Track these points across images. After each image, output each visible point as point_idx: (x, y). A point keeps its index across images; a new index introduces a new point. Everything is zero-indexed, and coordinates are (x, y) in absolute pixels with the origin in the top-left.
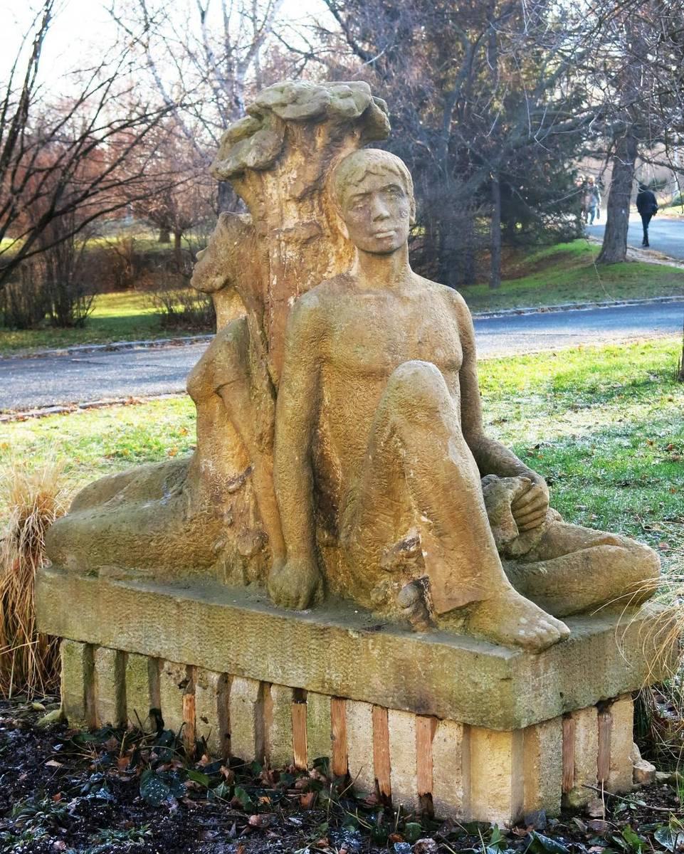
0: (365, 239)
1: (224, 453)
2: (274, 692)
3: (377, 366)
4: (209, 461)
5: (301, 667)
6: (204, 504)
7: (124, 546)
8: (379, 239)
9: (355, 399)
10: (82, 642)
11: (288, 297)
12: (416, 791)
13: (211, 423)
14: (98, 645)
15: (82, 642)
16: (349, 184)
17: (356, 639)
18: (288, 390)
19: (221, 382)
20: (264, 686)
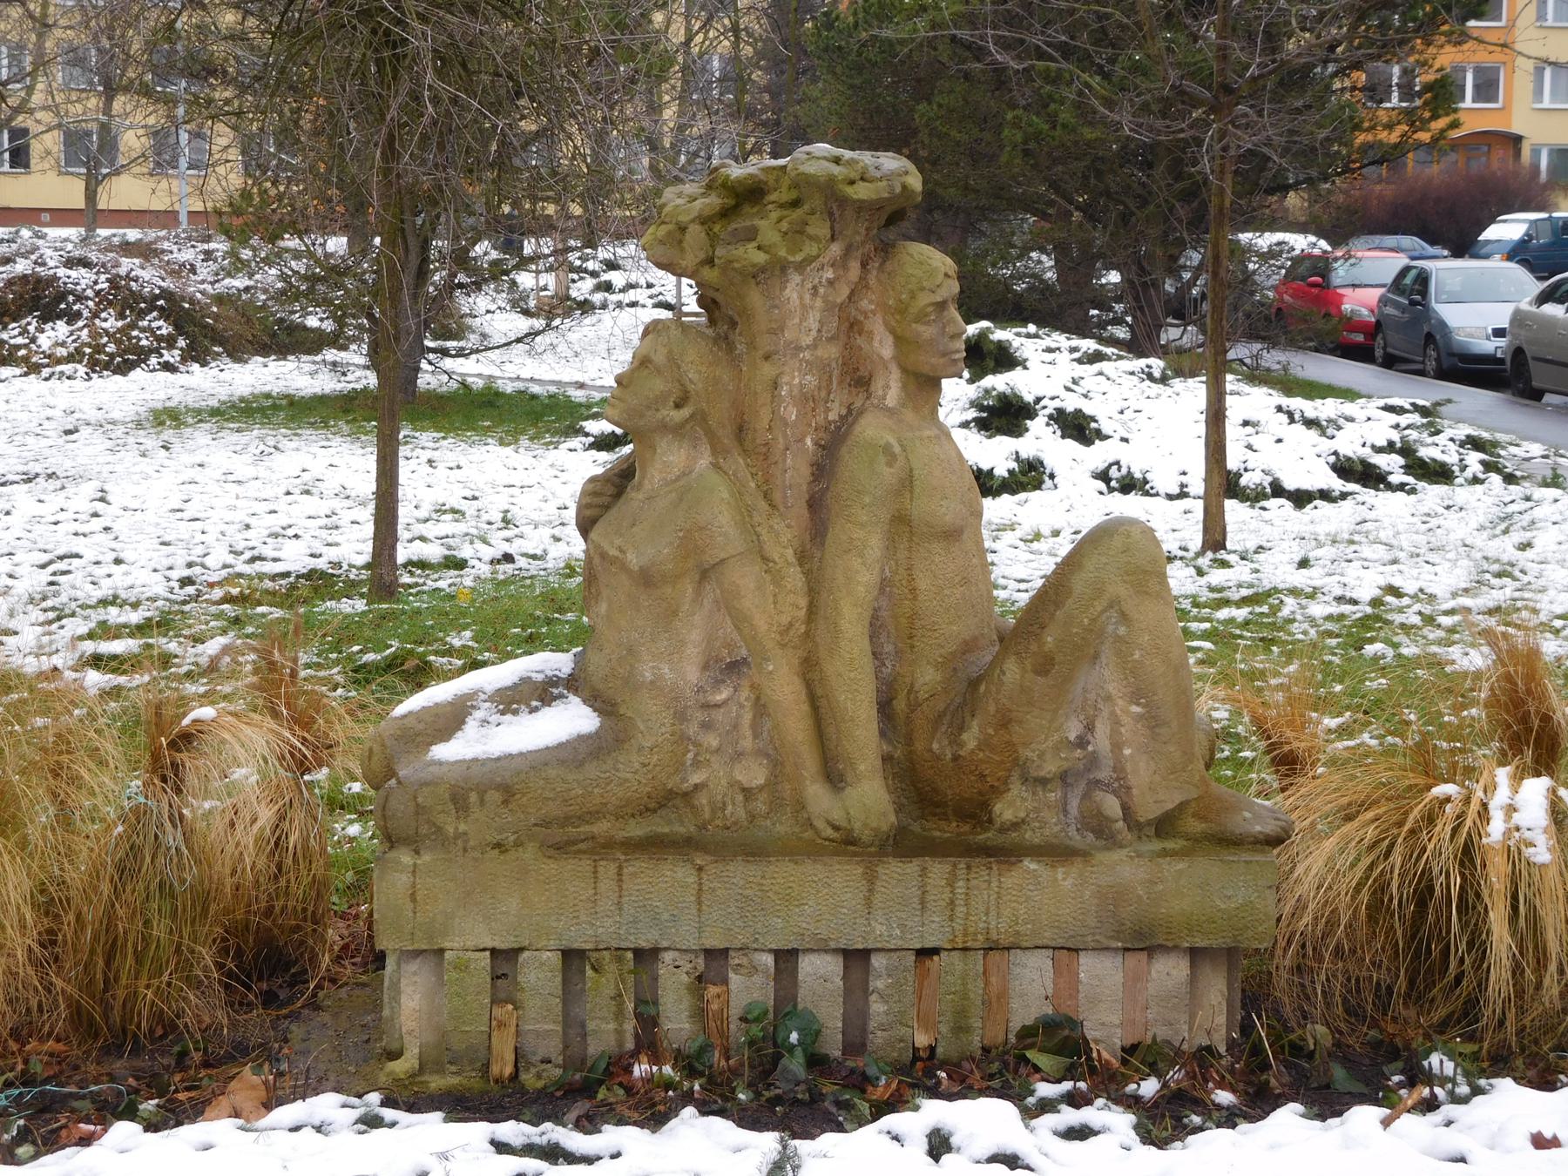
0: (933, 360)
1: (688, 652)
2: (810, 966)
3: (539, 552)
4: (662, 666)
5: (937, 919)
6: (664, 725)
7: (553, 800)
8: (955, 360)
9: (933, 567)
10: (484, 950)
11: (805, 436)
12: (1119, 1043)
13: (675, 613)
14: (522, 949)
15: (484, 950)
16: (922, 289)
17: (1035, 870)
18: (859, 560)
19: (723, 555)
20: (856, 959)
